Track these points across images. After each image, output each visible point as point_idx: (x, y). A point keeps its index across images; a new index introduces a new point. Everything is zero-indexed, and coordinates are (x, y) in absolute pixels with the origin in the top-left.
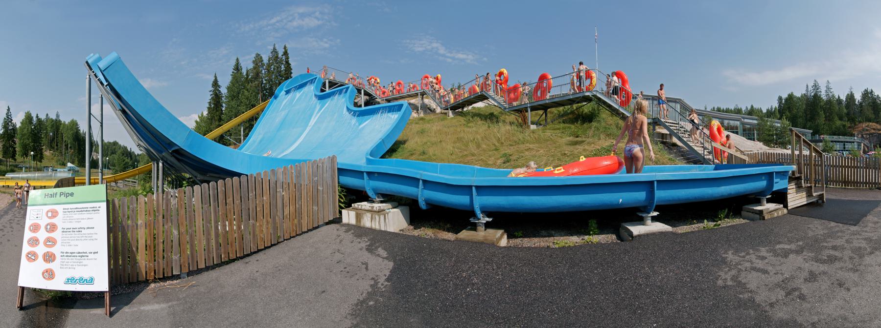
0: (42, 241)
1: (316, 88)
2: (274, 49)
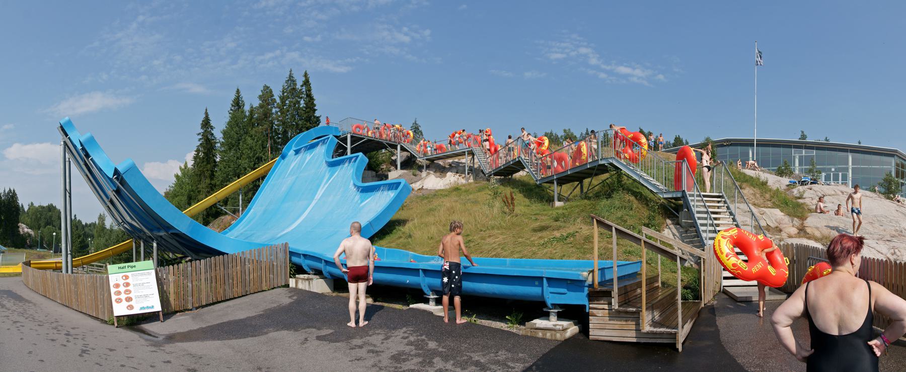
0: (123, 292)
1: (327, 151)
2: (291, 76)
